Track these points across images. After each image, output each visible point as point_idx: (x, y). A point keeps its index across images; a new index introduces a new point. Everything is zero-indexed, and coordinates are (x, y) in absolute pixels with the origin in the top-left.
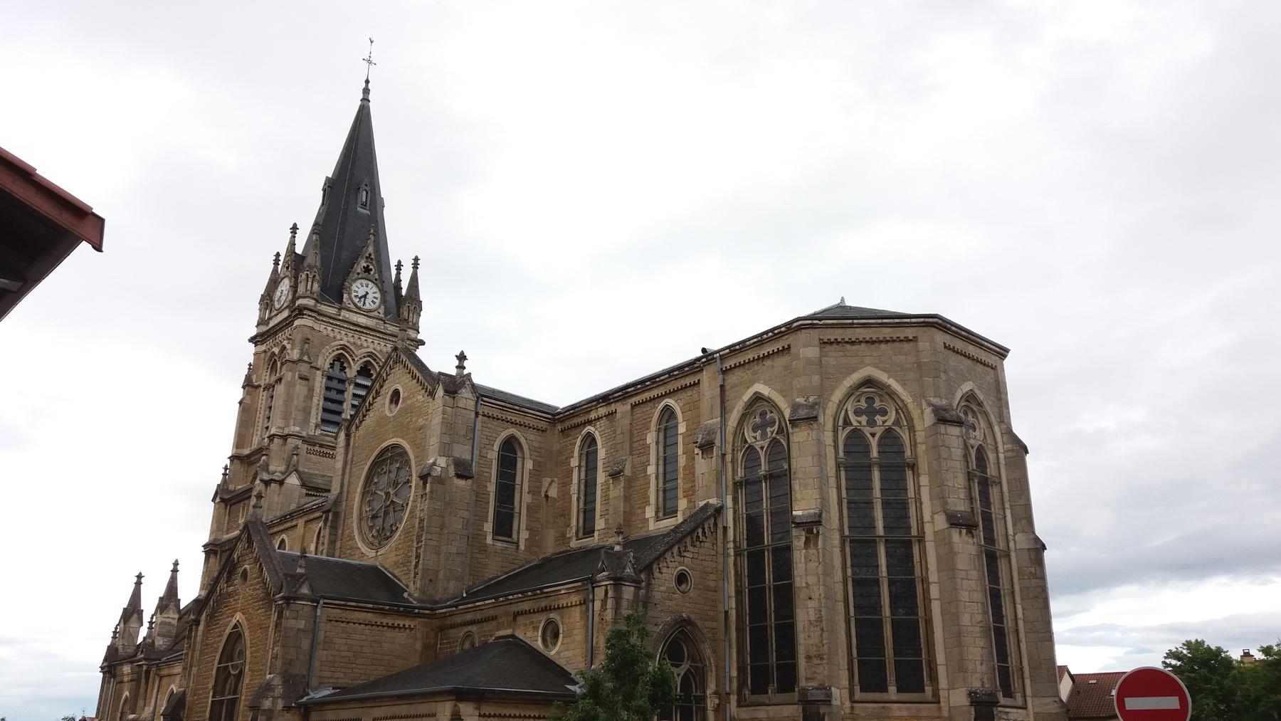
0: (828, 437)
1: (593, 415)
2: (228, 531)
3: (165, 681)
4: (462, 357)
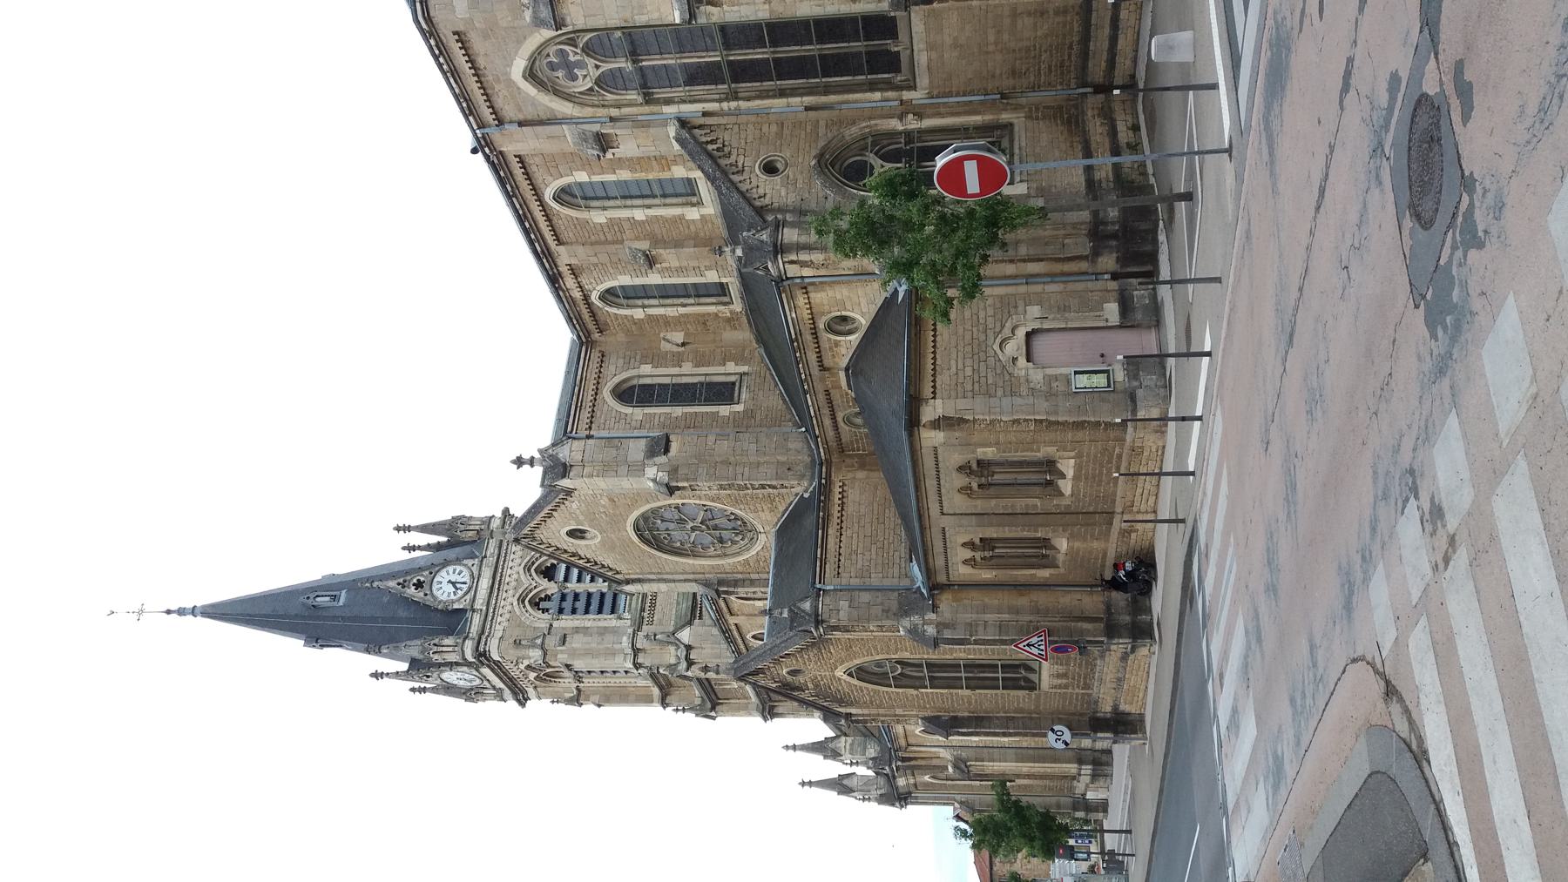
1: (577, 294)
2: (748, 698)
3: (911, 741)
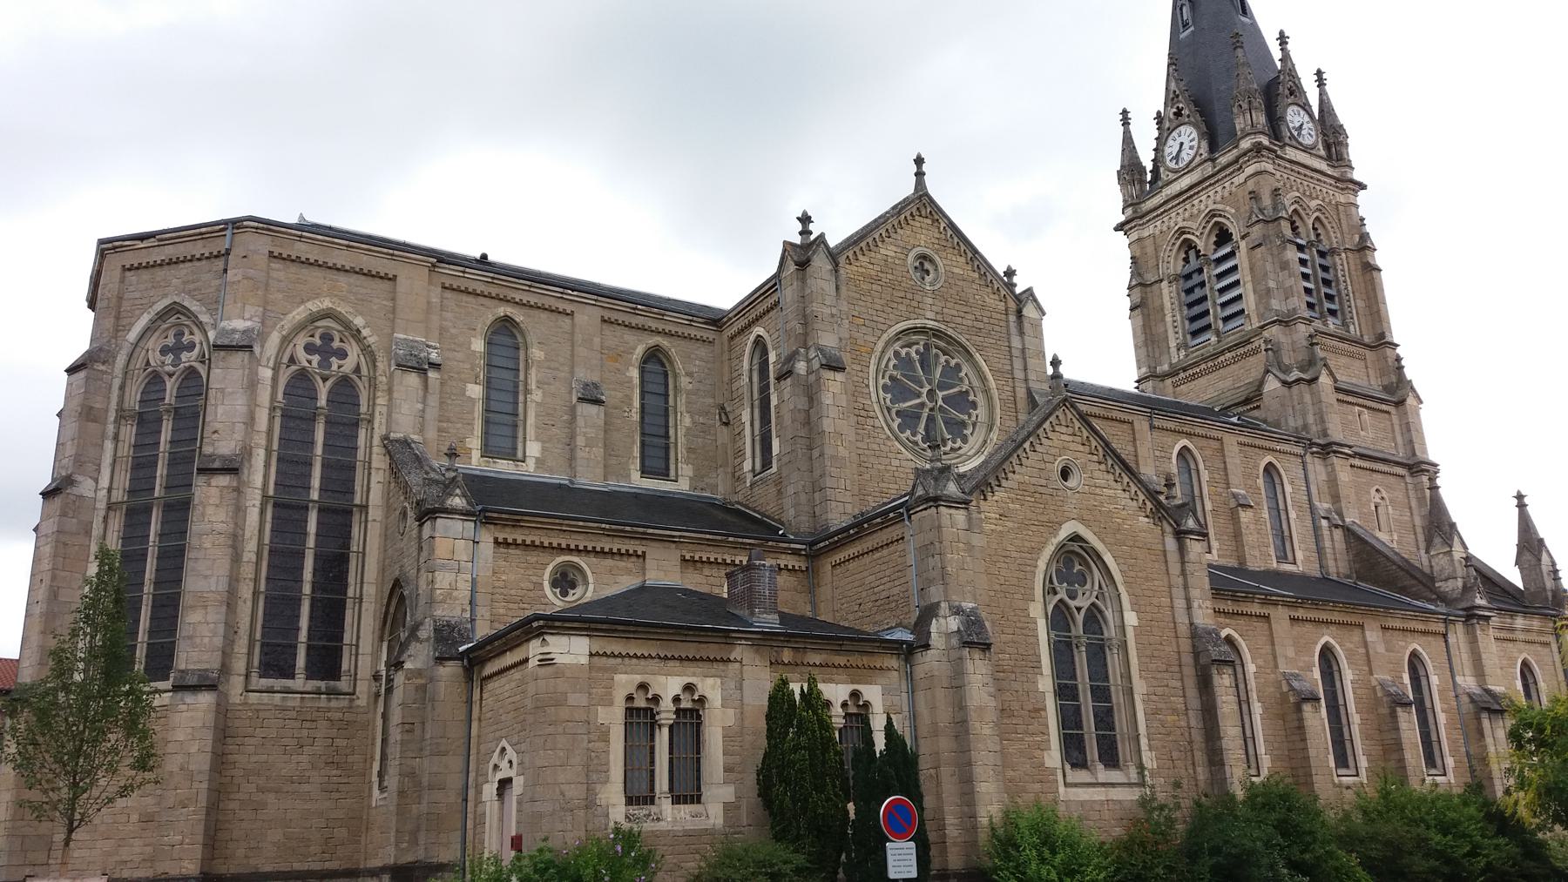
0: (266, 373)
4: (805, 219)
